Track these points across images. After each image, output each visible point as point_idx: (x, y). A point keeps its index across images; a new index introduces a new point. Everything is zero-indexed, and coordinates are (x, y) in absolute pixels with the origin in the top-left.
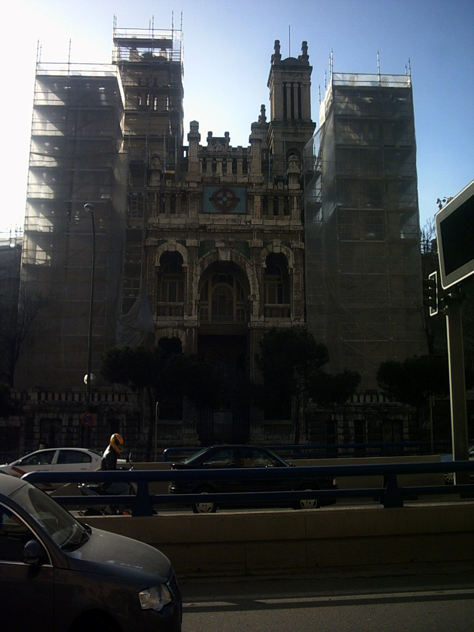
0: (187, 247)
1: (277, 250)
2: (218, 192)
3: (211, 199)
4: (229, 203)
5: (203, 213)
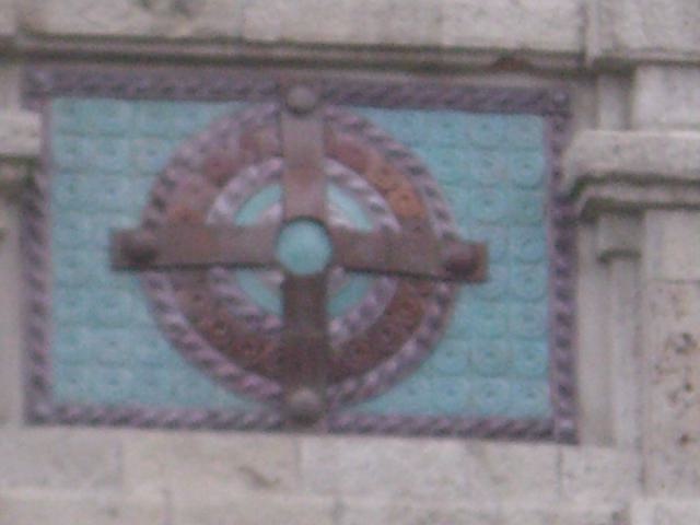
2: (219, 174)
3: (133, 257)
4: (258, 295)
5: (44, 408)
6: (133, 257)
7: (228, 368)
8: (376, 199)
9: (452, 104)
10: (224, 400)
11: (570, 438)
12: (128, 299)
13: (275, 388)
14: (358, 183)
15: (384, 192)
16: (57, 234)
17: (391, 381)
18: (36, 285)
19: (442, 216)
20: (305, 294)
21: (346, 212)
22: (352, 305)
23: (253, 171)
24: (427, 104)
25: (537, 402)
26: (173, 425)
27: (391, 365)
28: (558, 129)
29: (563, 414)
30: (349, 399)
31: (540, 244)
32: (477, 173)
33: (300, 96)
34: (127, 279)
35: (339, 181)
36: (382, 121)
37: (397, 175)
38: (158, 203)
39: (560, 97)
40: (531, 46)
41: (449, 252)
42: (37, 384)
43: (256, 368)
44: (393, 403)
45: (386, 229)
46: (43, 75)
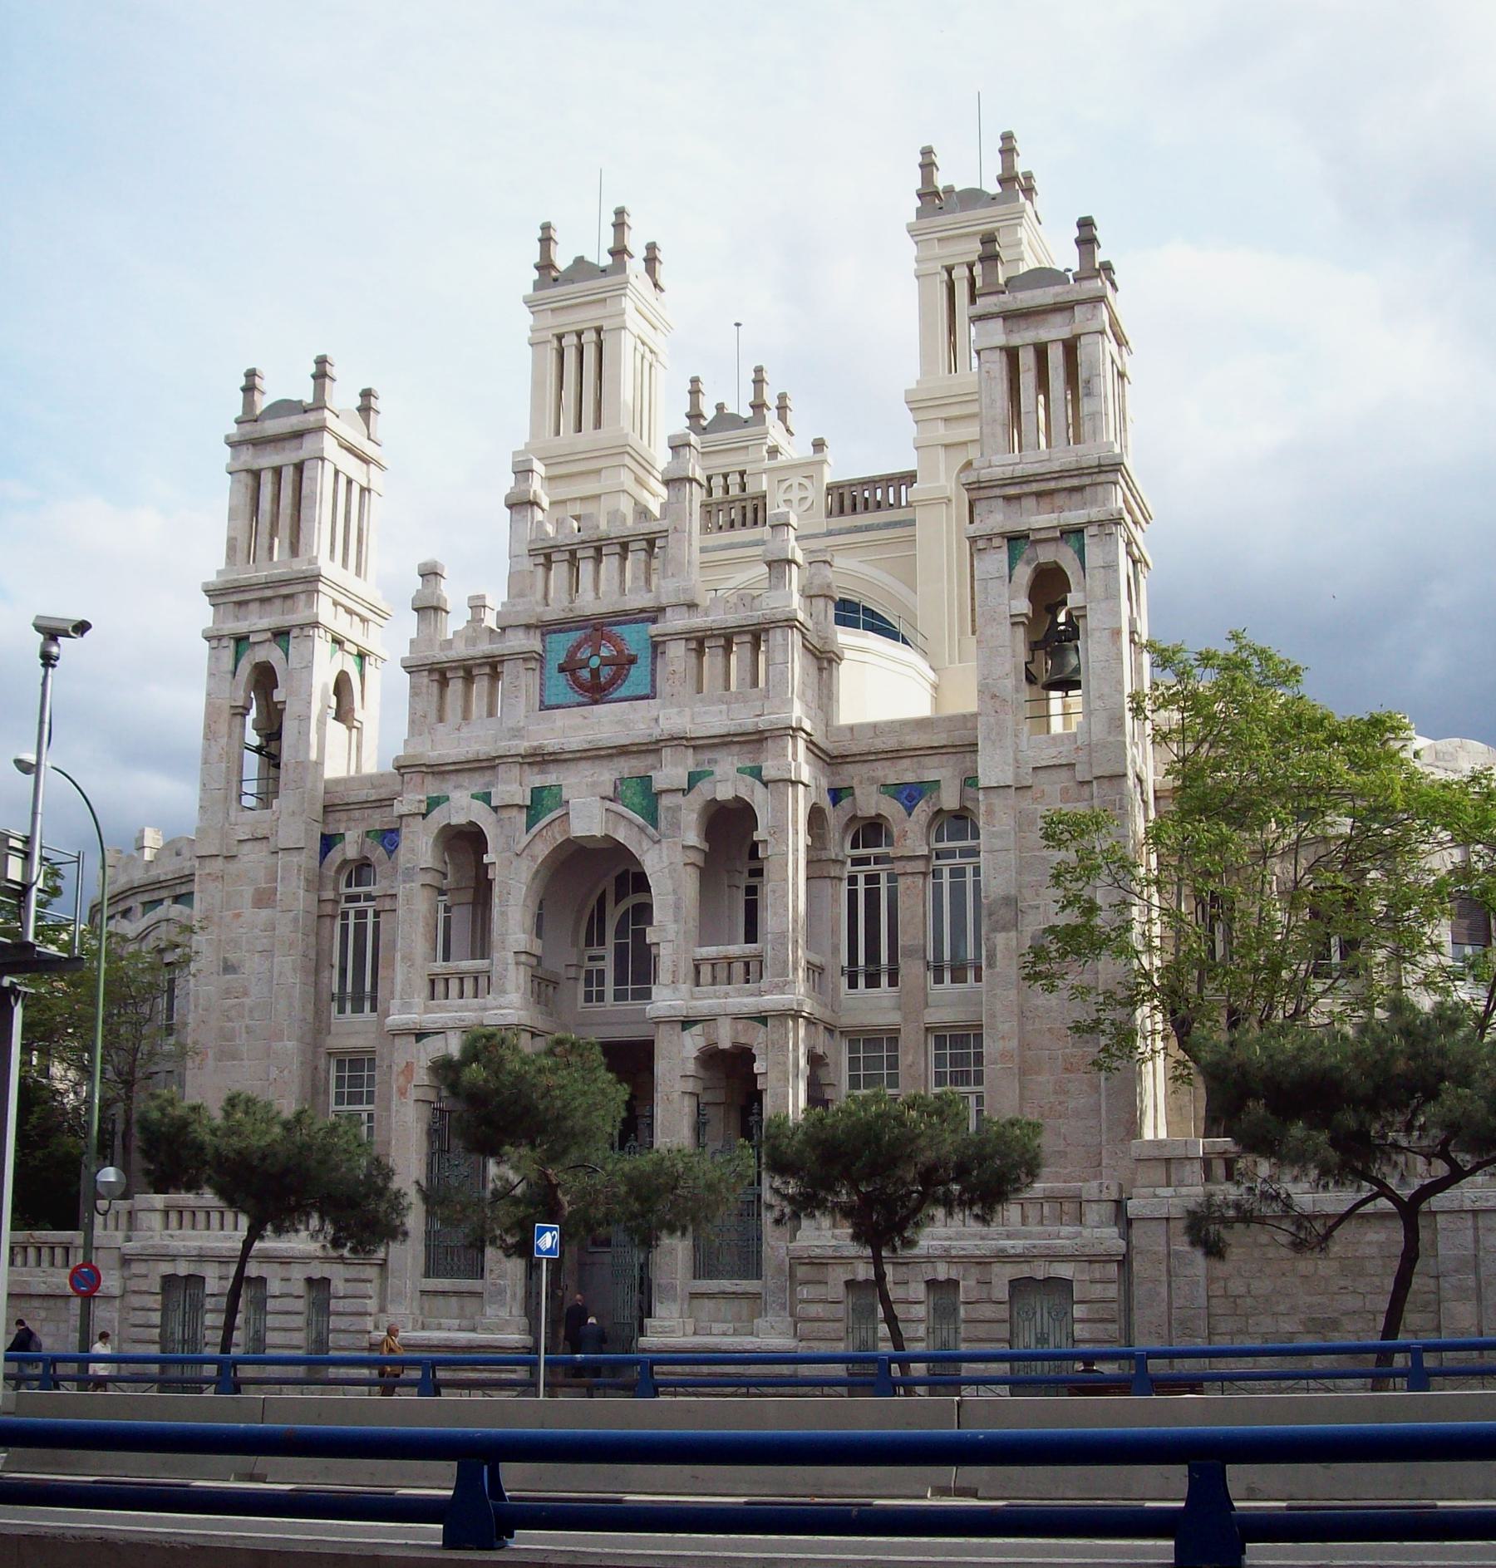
0: (495, 809)
1: (724, 793)
2: (579, 646)
4: (585, 674)
5: (544, 707)
6: (562, 669)
20: (595, 673)
21: (604, 652)
22: (606, 673)
25: (647, 691)
32: (633, 638)
42: (541, 702)
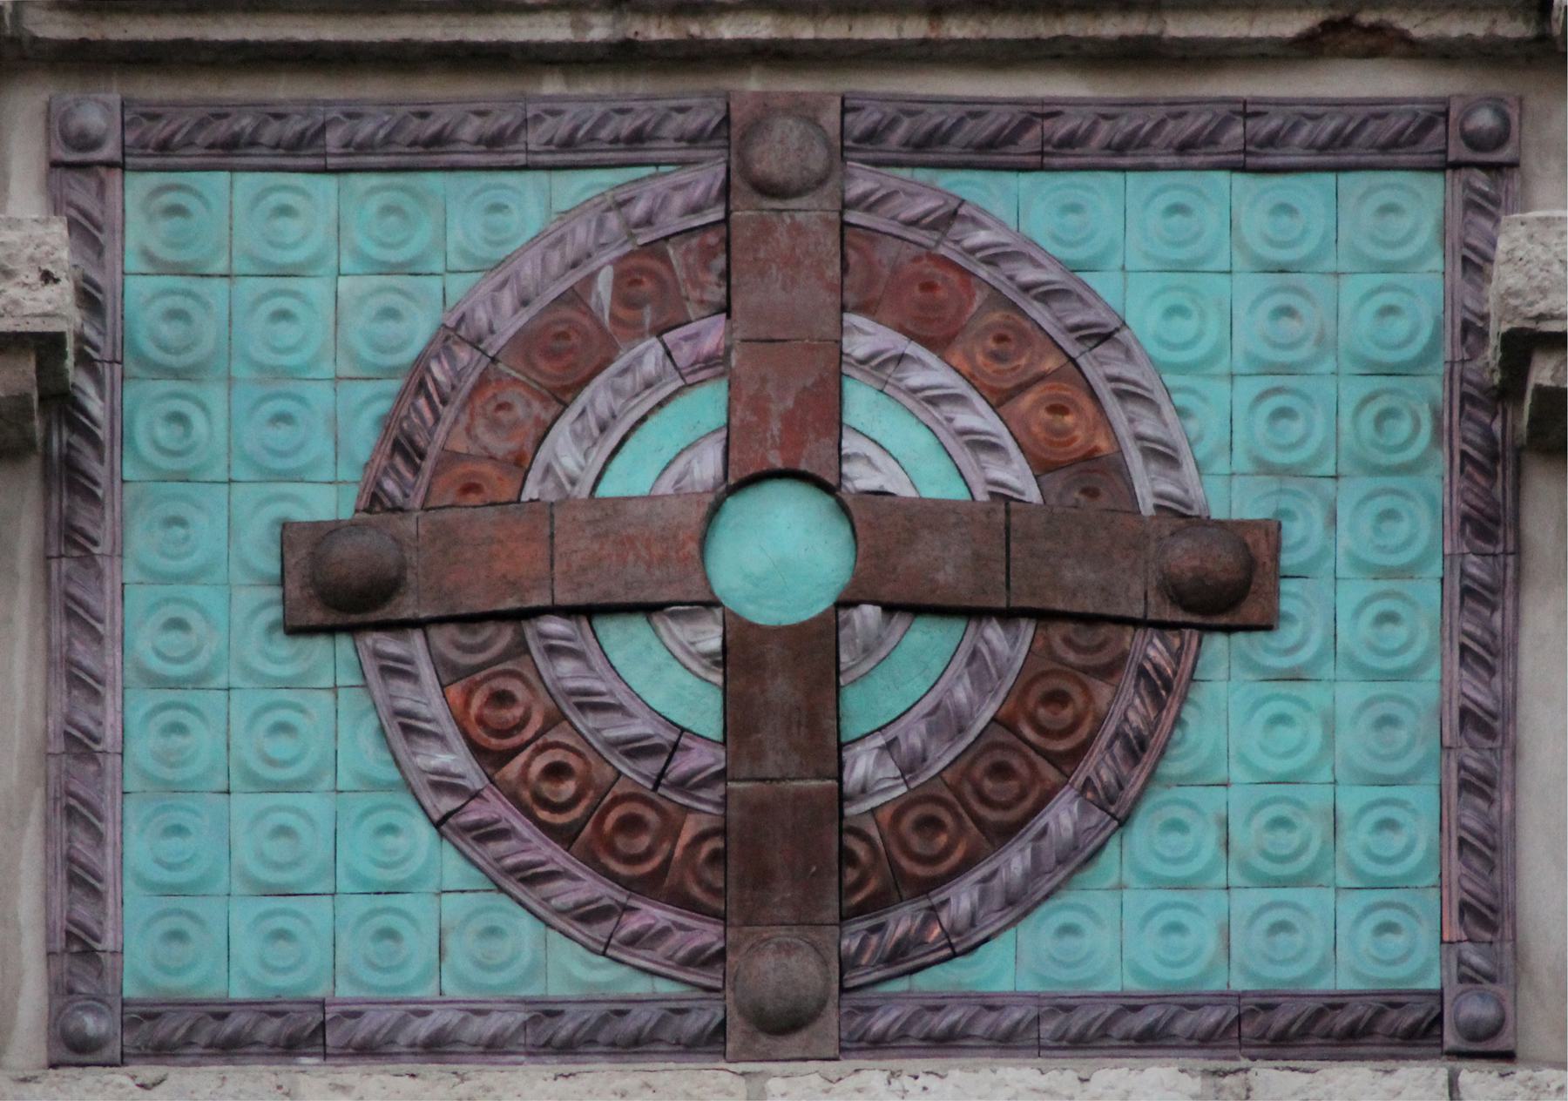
2: (561, 356)
4: (663, 680)
6: (337, 594)
7: (588, 888)
8: (980, 417)
9: (1193, 151)
10: (575, 972)
11: (1491, 1046)
12: (327, 710)
13: (707, 935)
14: (932, 373)
15: (999, 400)
16: (141, 541)
17: (1019, 903)
18: (82, 682)
19: (1164, 456)
20: (784, 676)
22: (910, 687)
23: (649, 355)
24: (1126, 153)
25: (1405, 952)
26: (437, 1047)
27: (1015, 861)
28: (1484, 206)
29: (1470, 977)
30: (902, 958)
31: (1420, 524)
33: (780, 151)
34: (331, 658)
35: (882, 366)
36: (1025, 211)
37: (1037, 355)
38: (403, 447)
39: (1484, 119)
40: (189, 19)
41: (1184, 556)
42: (79, 949)
43: (650, 887)
44: (1007, 966)
45: (1003, 498)
46: (97, 110)
